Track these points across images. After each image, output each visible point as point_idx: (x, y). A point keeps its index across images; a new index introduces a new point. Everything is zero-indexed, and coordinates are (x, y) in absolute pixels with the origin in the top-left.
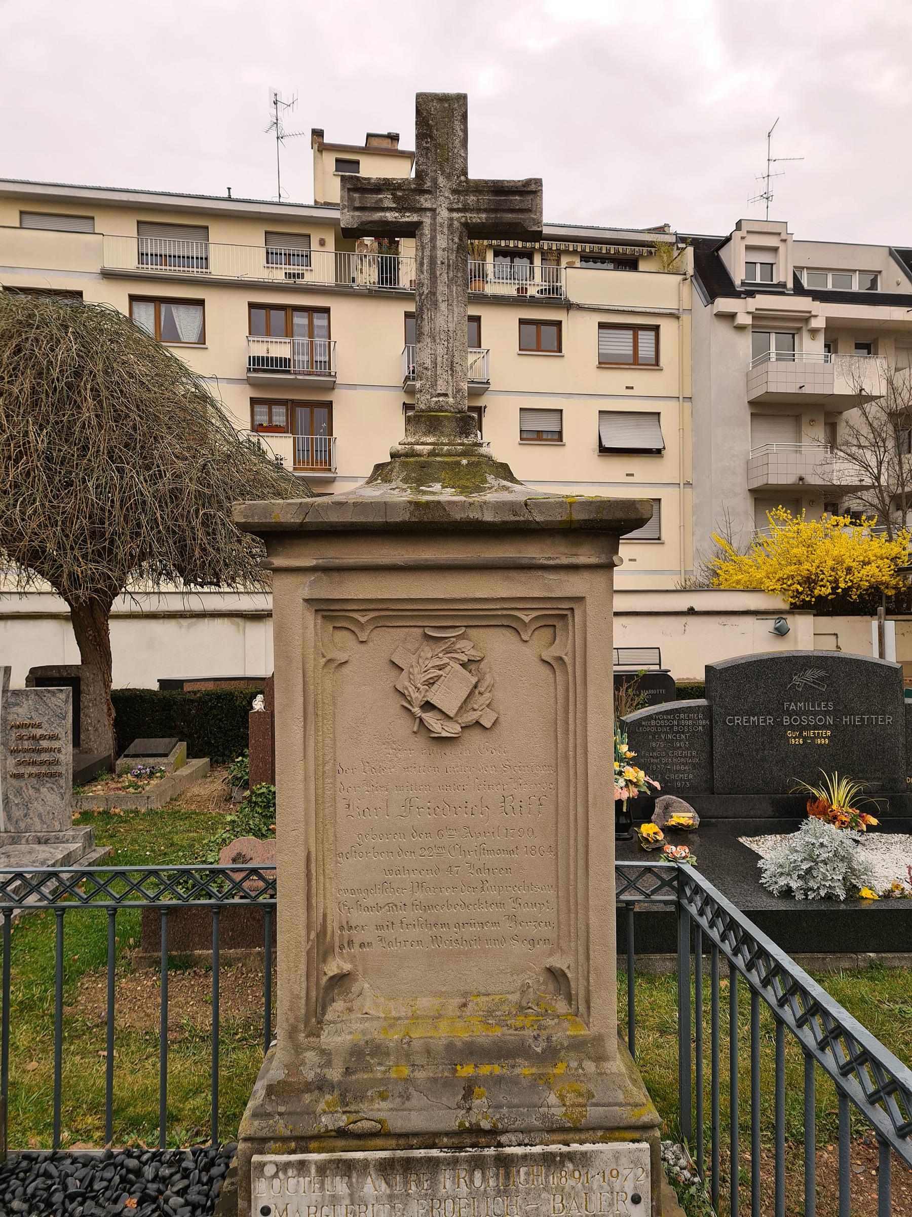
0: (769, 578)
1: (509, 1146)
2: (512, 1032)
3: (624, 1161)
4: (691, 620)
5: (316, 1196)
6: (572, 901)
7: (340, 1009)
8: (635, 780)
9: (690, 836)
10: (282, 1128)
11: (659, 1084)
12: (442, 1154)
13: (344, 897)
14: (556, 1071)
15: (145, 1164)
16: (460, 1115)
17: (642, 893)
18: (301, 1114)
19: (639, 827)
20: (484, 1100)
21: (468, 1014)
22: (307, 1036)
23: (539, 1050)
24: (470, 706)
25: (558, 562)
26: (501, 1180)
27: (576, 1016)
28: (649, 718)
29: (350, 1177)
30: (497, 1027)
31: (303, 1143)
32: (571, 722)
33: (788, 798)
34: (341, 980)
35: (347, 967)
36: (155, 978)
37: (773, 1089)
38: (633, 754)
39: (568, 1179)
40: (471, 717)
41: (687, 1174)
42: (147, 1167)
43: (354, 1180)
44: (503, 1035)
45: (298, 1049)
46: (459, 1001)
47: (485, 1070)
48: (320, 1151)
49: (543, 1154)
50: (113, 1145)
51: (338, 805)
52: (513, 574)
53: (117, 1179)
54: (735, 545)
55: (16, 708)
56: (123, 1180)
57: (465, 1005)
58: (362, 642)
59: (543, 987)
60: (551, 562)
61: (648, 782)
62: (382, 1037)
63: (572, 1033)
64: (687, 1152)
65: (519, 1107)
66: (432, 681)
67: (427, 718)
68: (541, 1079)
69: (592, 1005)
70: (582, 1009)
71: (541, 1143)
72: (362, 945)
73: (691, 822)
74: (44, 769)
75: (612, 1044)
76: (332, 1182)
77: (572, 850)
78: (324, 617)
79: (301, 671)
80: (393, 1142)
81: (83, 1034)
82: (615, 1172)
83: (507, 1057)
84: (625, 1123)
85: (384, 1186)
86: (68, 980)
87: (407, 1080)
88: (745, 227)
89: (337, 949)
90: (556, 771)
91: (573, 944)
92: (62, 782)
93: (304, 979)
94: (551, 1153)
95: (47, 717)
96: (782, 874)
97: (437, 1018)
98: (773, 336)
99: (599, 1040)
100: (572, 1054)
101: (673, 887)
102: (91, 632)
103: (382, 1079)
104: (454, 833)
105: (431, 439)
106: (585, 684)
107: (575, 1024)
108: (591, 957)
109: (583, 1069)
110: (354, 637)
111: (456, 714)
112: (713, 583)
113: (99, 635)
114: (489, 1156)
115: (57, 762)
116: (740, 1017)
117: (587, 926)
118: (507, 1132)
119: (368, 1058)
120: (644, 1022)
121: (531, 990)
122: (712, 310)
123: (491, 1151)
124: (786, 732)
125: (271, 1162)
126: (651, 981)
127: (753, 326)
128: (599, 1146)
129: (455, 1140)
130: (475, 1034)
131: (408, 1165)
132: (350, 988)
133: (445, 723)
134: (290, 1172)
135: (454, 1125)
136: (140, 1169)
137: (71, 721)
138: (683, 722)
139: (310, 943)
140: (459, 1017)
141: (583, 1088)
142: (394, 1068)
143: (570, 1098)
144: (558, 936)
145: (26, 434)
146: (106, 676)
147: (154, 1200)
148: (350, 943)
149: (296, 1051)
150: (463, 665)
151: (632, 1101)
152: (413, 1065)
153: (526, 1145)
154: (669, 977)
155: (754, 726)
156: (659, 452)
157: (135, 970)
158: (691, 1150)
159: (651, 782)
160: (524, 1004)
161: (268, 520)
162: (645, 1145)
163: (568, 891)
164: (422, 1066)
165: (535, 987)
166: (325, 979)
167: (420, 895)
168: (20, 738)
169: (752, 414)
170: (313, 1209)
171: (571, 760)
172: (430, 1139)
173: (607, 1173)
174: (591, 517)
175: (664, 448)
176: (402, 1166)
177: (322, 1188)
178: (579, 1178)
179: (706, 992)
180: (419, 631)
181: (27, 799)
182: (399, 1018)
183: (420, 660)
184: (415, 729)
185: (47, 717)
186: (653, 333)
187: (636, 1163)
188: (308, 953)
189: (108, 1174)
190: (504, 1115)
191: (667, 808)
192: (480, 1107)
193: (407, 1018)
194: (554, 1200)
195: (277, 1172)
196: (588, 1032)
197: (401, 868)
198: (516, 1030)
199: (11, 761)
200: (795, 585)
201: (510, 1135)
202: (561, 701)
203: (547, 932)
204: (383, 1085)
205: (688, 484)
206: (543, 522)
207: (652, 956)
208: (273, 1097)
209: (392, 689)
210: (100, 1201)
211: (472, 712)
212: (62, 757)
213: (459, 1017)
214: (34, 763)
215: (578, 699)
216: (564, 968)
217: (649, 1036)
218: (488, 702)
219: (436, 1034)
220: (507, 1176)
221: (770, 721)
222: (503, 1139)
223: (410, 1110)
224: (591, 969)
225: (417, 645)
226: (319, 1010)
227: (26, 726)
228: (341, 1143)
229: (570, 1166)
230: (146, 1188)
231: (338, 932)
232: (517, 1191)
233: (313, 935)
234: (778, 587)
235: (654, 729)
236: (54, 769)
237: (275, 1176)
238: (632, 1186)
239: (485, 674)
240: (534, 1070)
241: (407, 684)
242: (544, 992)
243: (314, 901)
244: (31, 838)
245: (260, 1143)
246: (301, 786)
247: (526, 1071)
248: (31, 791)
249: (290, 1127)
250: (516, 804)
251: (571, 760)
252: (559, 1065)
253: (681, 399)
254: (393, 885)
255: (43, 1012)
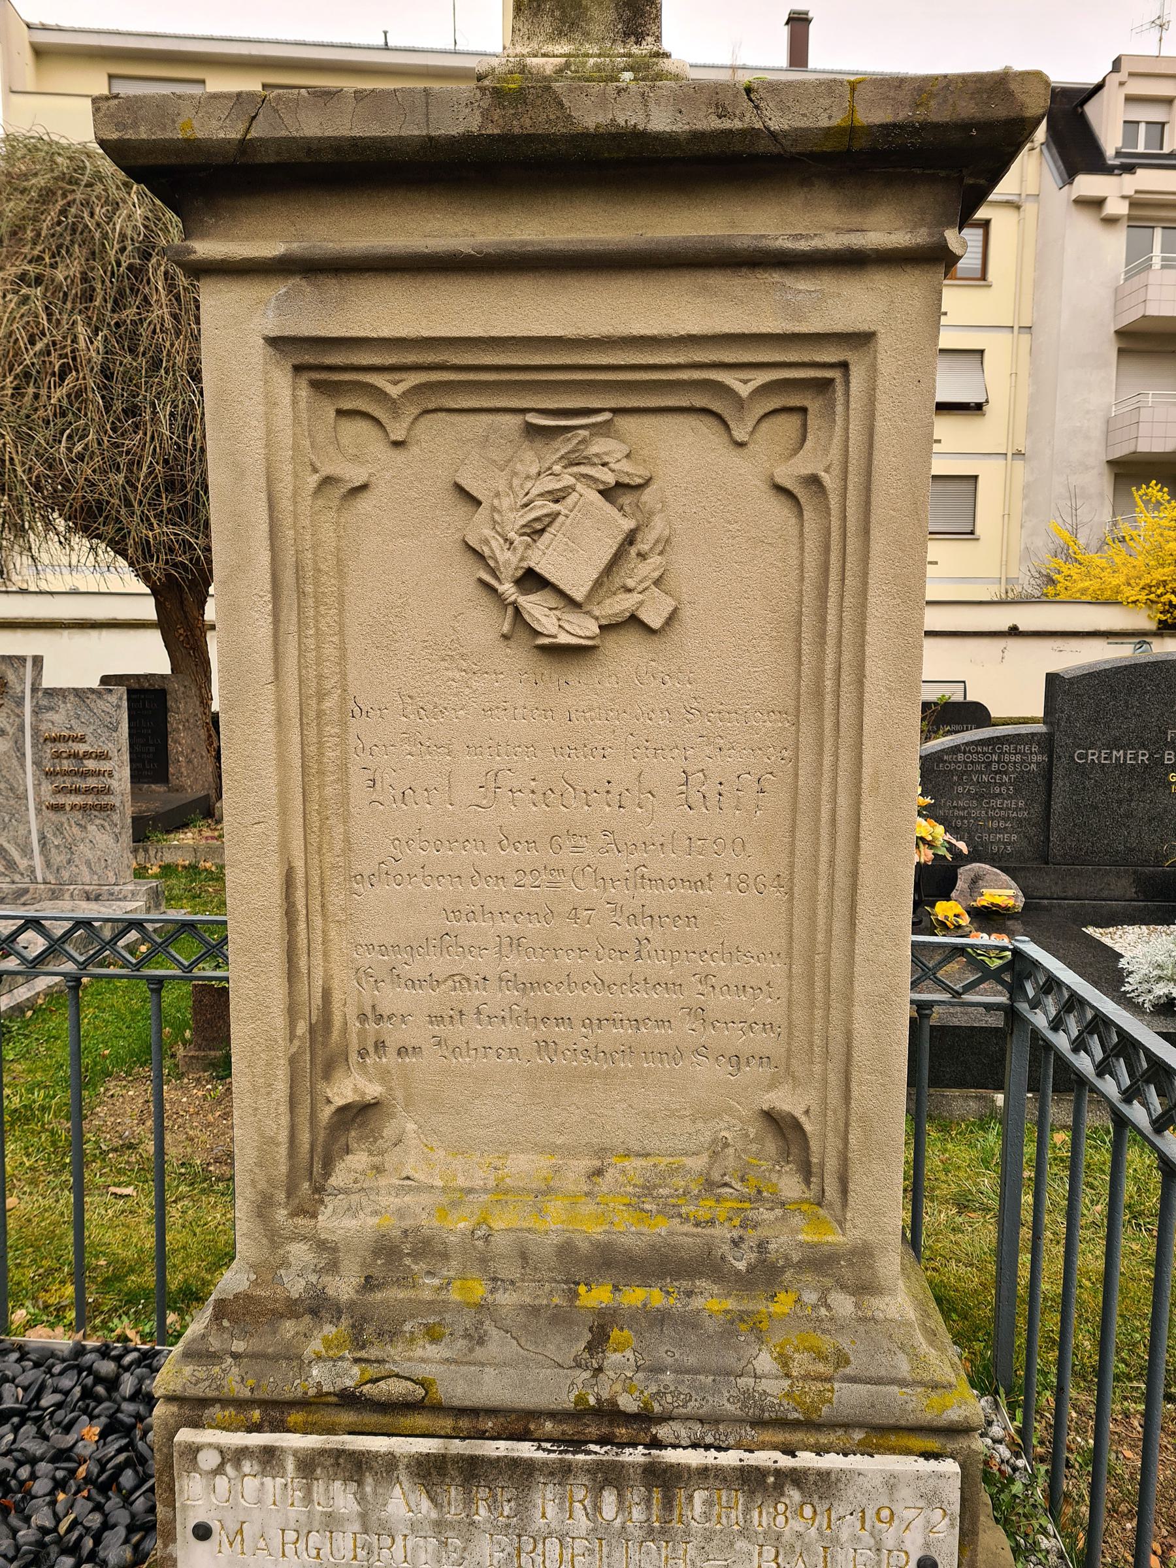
0: (1129, 584)
1: (675, 1447)
2: (688, 1228)
3: (905, 1493)
4: (1013, 644)
5: (297, 1511)
6: (819, 984)
7: (360, 1168)
8: (929, 838)
9: (1009, 923)
10: (235, 1382)
11: (957, 1290)
12: (541, 1455)
13: (366, 959)
14: (775, 1308)
15: (127, 1369)
16: (579, 1381)
17: (947, 988)
18: (275, 1358)
19: (933, 906)
20: (629, 1354)
21: (605, 1189)
22: (293, 1215)
23: (741, 1266)
24: (618, 581)
25: (818, 243)
26: (655, 1510)
27: (819, 1204)
28: (955, 750)
29: (360, 1483)
30: (660, 1218)
31: (275, 1413)
32: (831, 617)
33: (1164, 872)
34: (359, 1115)
35: (373, 1090)
36: (209, 1086)
37: (1148, 1310)
38: (928, 800)
39: (788, 1517)
40: (617, 606)
41: (1004, 1451)
42: (127, 1375)
43: (368, 1489)
44: (671, 1233)
45: (274, 1238)
46: (587, 1163)
47: (634, 1296)
48: (306, 1429)
49: (742, 1469)
50: (85, 1337)
51: (353, 779)
52: (717, 280)
53: (77, 1391)
54: (1082, 541)
55: (51, 713)
56: (87, 1393)
57: (599, 1172)
58: (397, 444)
59: (754, 1147)
60: (803, 245)
61: (949, 843)
62: (436, 1223)
63: (808, 1238)
64: (1004, 1411)
65: (698, 1373)
66: (538, 526)
67: (528, 606)
68: (742, 1320)
69: (851, 1186)
70: (832, 1193)
71: (738, 1446)
72: (402, 1051)
73: (1011, 902)
74: (90, 800)
75: (892, 1261)
76: (327, 1489)
77: (822, 884)
78: (315, 385)
79: (263, 496)
80: (447, 1423)
81: (94, 1161)
82: (885, 1513)
83: (677, 1275)
84: (911, 1420)
85: (425, 1504)
86: (87, 1084)
87: (481, 1307)
88: (1126, 68)
89: (354, 1057)
90: (797, 724)
91: (817, 1068)
92: (116, 817)
93: (284, 1108)
94: (757, 1468)
95: (92, 727)
96: (1160, 978)
97: (544, 1193)
98: (1158, 232)
99: (863, 1254)
100: (808, 1277)
101: (1002, 982)
102: (181, 631)
103: (432, 1302)
104: (582, 842)
105: (564, 48)
106: (866, 532)
107: (816, 1221)
108: (855, 1094)
109: (828, 1307)
110: (380, 434)
111: (590, 596)
112: (1048, 589)
113: (193, 636)
114: (633, 1465)
115: (107, 791)
116: (1088, 1190)
117: (849, 1034)
118: (671, 1418)
119: (408, 1261)
120: (933, 1189)
121: (731, 1151)
122: (1069, 196)
123: (636, 1456)
124: (1167, 774)
125: (210, 1445)
126: (944, 1129)
127: (1130, 218)
128: (856, 1462)
129: (568, 1429)
130: (616, 1229)
131: (473, 1471)
132: (380, 1131)
133: (565, 617)
134: (247, 1467)
135: (567, 1401)
136: (118, 1377)
137: (126, 734)
138: (1007, 757)
139: (297, 1043)
140: (587, 1194)
141: (826, 1343)
142: (458, 1283)
143: (801, 1363)
144: (789, 1050)
145: (75, 340)
146: (203, 691)
147: (128, 1430)
148: (380, 1045)
149: (272, 1241)
150: (607, 493)
151: (926, 1377)
152: (495, 1279)
153: (707, 1447)
154: (974, 1124)
155: (1118, 765)
156: (979, 407)
157: (183, 1074)
158: (1012, 1407)
159: (954, 841)
160: (716, 1176)
161: (168, 135)
162: (951, 1467)
163: (810, 963)
164: (512, 1283)
165: (739, 1146)
166: (326, 1113)
167: (514, 962)
168: (58, 755)
169: (1121, 351)
170: (291, 1535)
171: (829, 698)
172: (518, 1423)
173: (870, 1513)
174: (901, 118)
175: (987, 401)
176: (461, 1471)
177: (308, 1498)
178: (813, 1519)
179: (1030, 1150)
180: (514, 421)
181: (70, 840)
182: (471, 1191)
183: (507, 471)
184: (506, 628)
185: (92, 727)
186: (980, 231)
187: (931, 1499)
188: (293, 1061)
189: (66, 1382)
190: (666, 1387)
191: (975, 881)
192: (617, 1367)
193: (486, 1191)
194: (760, 1554)
195: (222, 1464)
196: (841, 1239)
197: (477, 909)
198: (697, 1225)
199: (47, 787)
200: (1168, 596)
201: (676, 1426)
202: (811, 573)
203: (764, 1042)
204: (434, 1313)
205: (1019, 454)
206: (785, 134)
207: (948, 1092)
208: (226, 1323)
209: (459, 546)
210: (44, 1427)
211: (622, 596)
212: (114, 784)
213: (587, 1194)
214: (77, 791)
215: (848, 565)
216: (798, 1113)
217: (940, 1212)
218: (656, 574)
219: (539, 1225)
220: (668, 1504)
221: (1143, 757)
222: (663, 1432)
223: (483, 1365)
224: (853, 1118)
225: (510, 452)
226: (317, 1168)
227: (65, 739)
228: (347, 1417)
229: (795, 1495)
230: (118, 1410)
231: (355, 1026)
232: (687, 1532)
233: (302, 1028)
234: (1143, 597)
235: (962, 767)
236: (105, 800)
237: (219, 1470)
238: (920, 1541)
239: (651, 513)
240: (730, 1304)
241: (487, 532)
242: (757, 1156)
243: (303, 963)
244: (76, 892)
245: (195, 1409)
246: (271, 735)
247: (715, 1305)
248: (76, 830)
249: (251, 1382)
250: (711, 789)
251: (829, 698)
252: (782, 1296)
253: (1016, 328)
254: (461, 940)
255: (43, 1126)
